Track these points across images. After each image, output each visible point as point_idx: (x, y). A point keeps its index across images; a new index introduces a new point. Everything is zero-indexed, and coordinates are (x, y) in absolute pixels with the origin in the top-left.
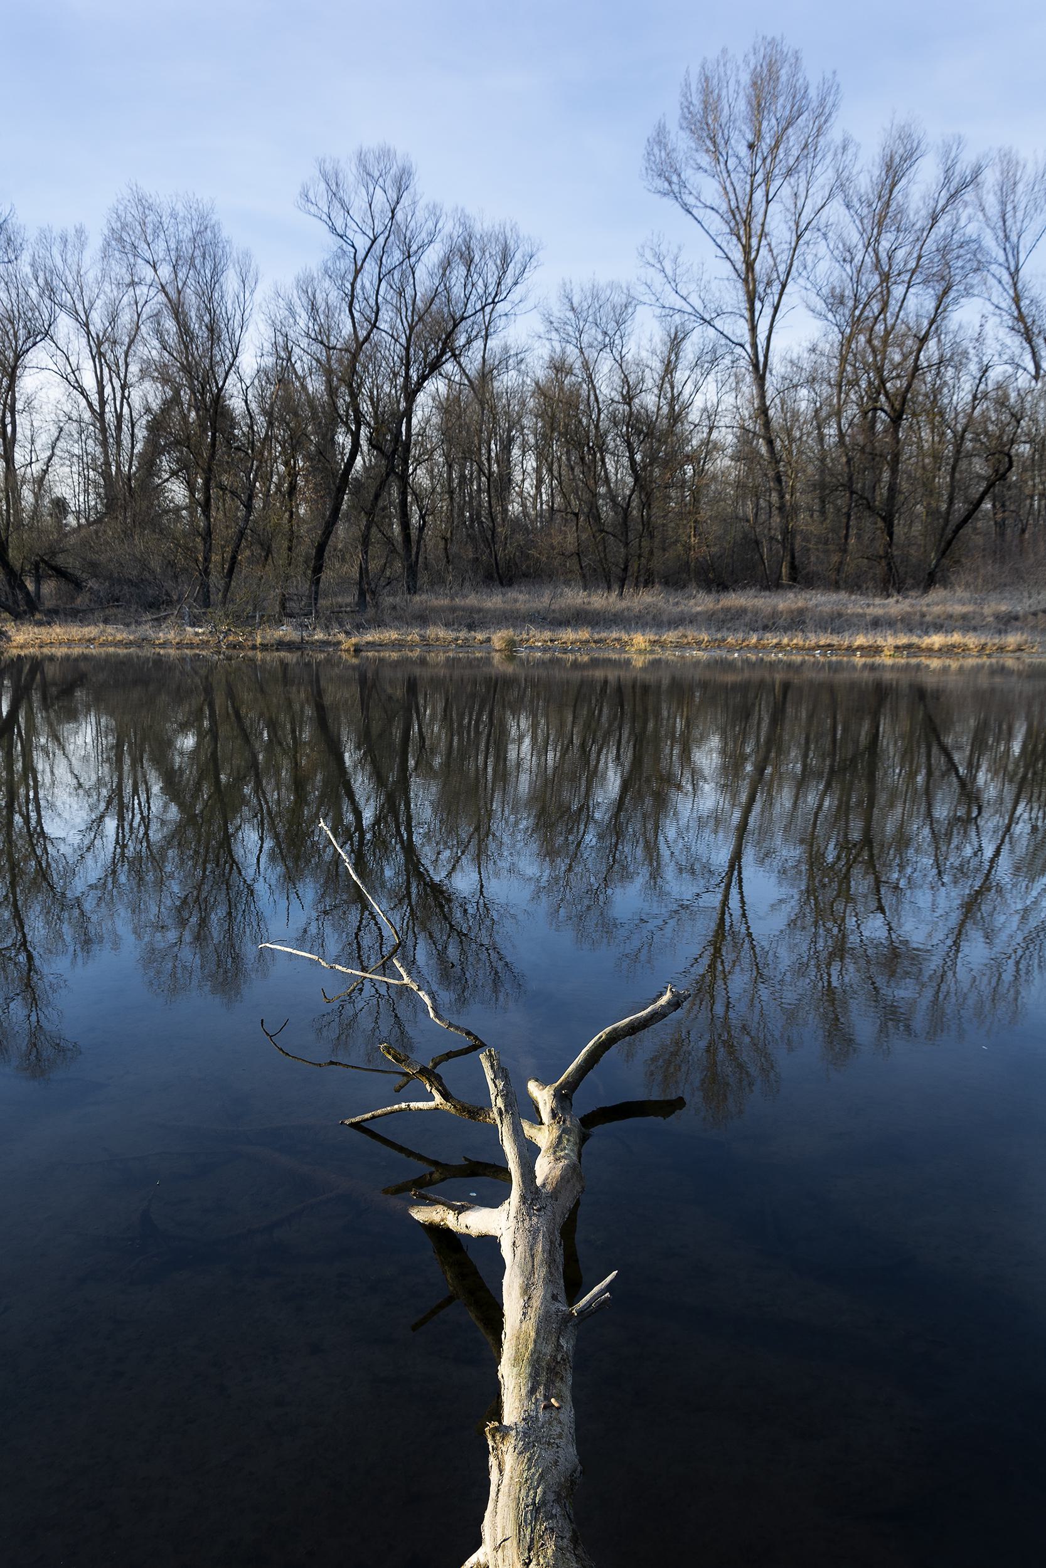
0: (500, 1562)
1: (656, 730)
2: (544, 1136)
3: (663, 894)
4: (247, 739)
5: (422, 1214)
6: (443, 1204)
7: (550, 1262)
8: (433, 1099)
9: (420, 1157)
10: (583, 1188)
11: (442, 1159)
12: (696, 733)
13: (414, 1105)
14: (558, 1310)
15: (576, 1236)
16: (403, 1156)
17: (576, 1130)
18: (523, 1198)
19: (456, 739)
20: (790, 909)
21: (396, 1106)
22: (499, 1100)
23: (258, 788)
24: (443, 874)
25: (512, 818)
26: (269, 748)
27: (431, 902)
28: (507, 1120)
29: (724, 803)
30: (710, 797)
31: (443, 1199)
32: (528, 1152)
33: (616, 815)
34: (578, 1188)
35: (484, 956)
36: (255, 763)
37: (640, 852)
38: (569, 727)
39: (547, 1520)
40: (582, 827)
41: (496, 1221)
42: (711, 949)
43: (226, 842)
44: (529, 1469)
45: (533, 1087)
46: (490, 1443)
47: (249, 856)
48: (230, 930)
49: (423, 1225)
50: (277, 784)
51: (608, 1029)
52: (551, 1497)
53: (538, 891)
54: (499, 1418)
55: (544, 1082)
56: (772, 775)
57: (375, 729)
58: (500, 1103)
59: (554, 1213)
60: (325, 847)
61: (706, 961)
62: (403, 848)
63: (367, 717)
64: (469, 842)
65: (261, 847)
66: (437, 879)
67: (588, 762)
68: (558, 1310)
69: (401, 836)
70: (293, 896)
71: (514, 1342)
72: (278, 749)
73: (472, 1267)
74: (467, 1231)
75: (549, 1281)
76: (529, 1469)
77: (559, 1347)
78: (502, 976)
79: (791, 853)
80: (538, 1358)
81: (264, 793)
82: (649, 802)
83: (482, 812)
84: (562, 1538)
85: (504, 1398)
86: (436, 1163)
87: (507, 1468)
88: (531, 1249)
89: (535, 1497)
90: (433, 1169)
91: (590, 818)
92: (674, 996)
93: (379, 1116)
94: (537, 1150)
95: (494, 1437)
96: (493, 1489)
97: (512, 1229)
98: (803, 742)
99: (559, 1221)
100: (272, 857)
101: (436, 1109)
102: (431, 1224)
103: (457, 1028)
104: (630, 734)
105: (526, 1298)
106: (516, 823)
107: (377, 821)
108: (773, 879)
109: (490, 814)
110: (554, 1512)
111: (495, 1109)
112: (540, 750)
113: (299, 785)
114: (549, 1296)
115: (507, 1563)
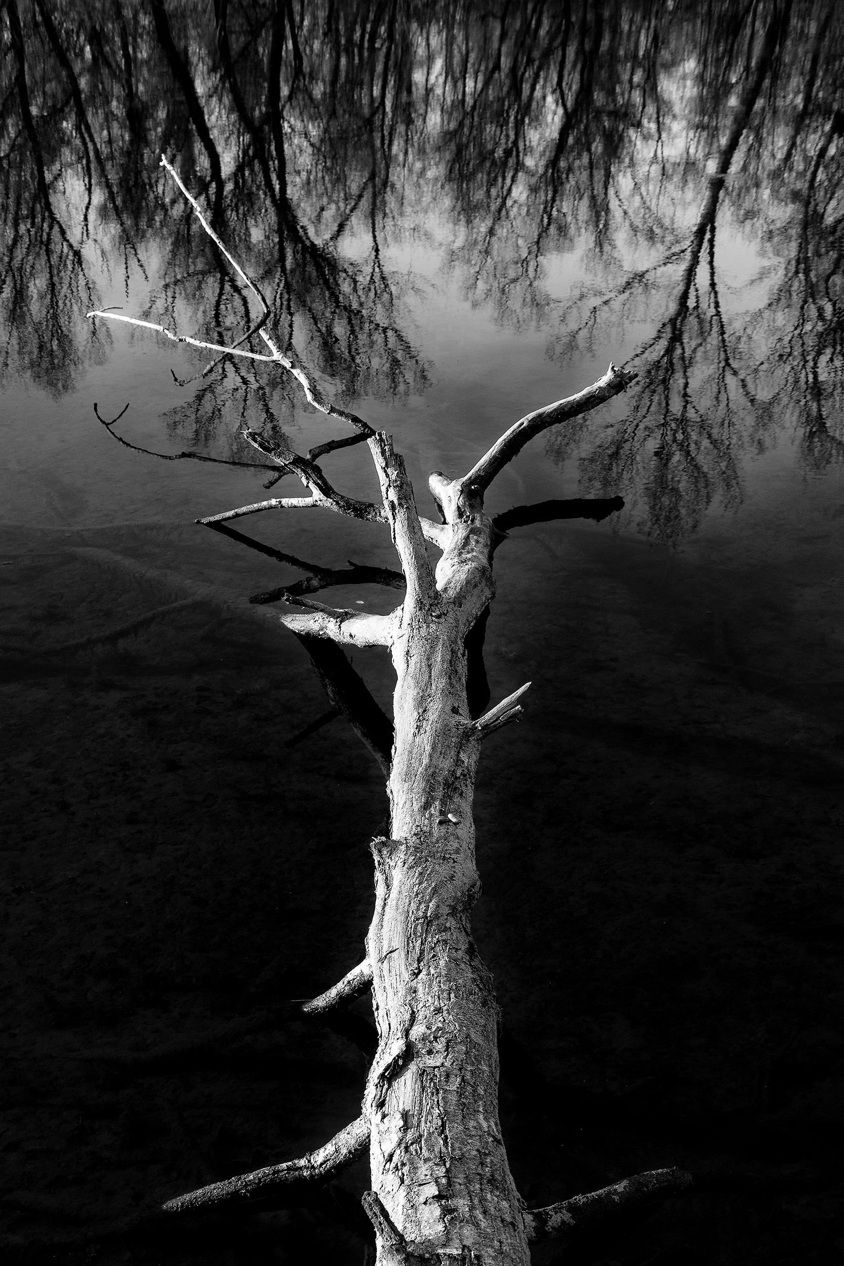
0: (386, 972)
1: (613, 51)
2: (447, 537)
3: (611, 263)
4: (66, 64)
5: (299, 623)
6: (322, 611)
7: (451, 673)
8: (310, 494)
9: (294, 561)
10: (493, 594)
11: (321, 564)
12: (665, 55)
13: (286, 502)
14: (458, 724)
15: (484, 648)
16: (274, 560)
17: (487, 530)
18: (420, 604)
19: (343, 61)
20: (777, 279)
21: (265, 503)
22: (391, 490)
23: (82, 123)
24: (327, 236)
25: (418, 165)
26: (94, 69)
27: (310, 273)
28: (401, 515)
29: (697, 151)
30: (679, 141)
31: (322, 606)
32: (427, 556)
33: (553, 163)
34: (488, 593)
35: (378, 337)
36: (76, 91)
37: (584, 206)
38: (495, 45)
39: (440, 932)
40: (508, 181)
41: (385, 629)
42: (668, 333)
43: (43, 191)
44: (420, 884)
45: (436, 483)
46: (376, 858)
47: (74, 212)
48: (53, 305)
49: (298, 635)
50: (107, 119)
51: (531, 416)
52: (445, 910)
53: (452, 256)
54: (387, 833)
55: (448, 476)
56: (763, 109)
57: (236, 43)
58: (393, 495)
59: (457, 621)
60: (173, 202)
61: (663, 343)
62: (274, 201)
63: (223, 28)
64: (360, 196)
65: (89, 203)
66: (318, 242)
67: (519, 92)
68: (458, 724)
69: (272, 190)
70: (133, 263)
71: (406, 757)
72: (105, 71)
73: (359, 682)
74: (352, 641)
75: (450, 692)
76: (420, 884)
77: (458, 762)
78: (401, 359)
79: (783, 213)
80: (434, 773)
81: (88, 128)
82: (598, 147)
83: (379, 156)
84: (457, 950)
85: (393, 814)
86: (315, 569)
87: (396, 884)
88: (428, 659)
89: (426, 910)
90: (311, 575)
91: (519, 166)
92: (616, 376)
93: (244, 514)
94: (437, 553)
95: (380, 851)
96: (379, 903)
97: (406, 637)
98: (808, 66)
99: (463, 629)
100: (103, 212)
101: (314, 506)
102: (308, 634)
103: (341, 413)
104: (577, 54)
105: (421, 711)
106: (423, 171)
107: (240, 169)
108: (755, 245)
109: (388, 159)
110: (448, 925)
111: (386, 503)
112: (456, 76)
113: (136, 118)
114: (448, 709)
115: (393, 973)
